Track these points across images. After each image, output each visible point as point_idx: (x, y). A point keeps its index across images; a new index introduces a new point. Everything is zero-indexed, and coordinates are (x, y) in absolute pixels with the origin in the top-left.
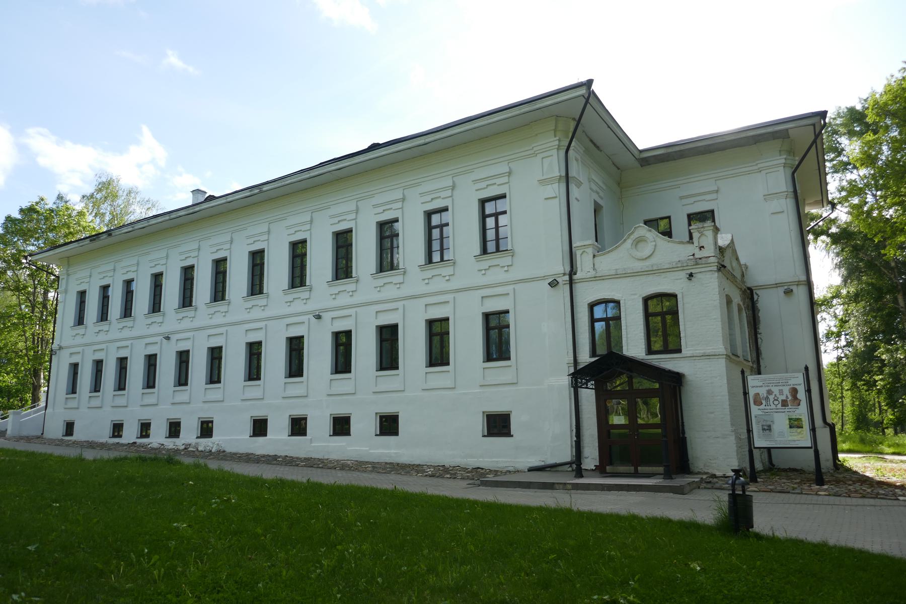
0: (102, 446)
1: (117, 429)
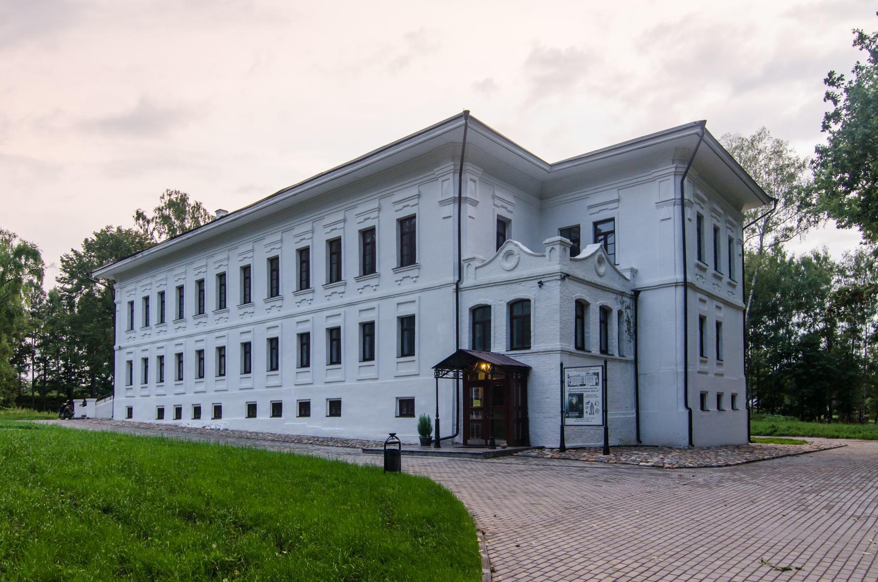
0: (149, 427)
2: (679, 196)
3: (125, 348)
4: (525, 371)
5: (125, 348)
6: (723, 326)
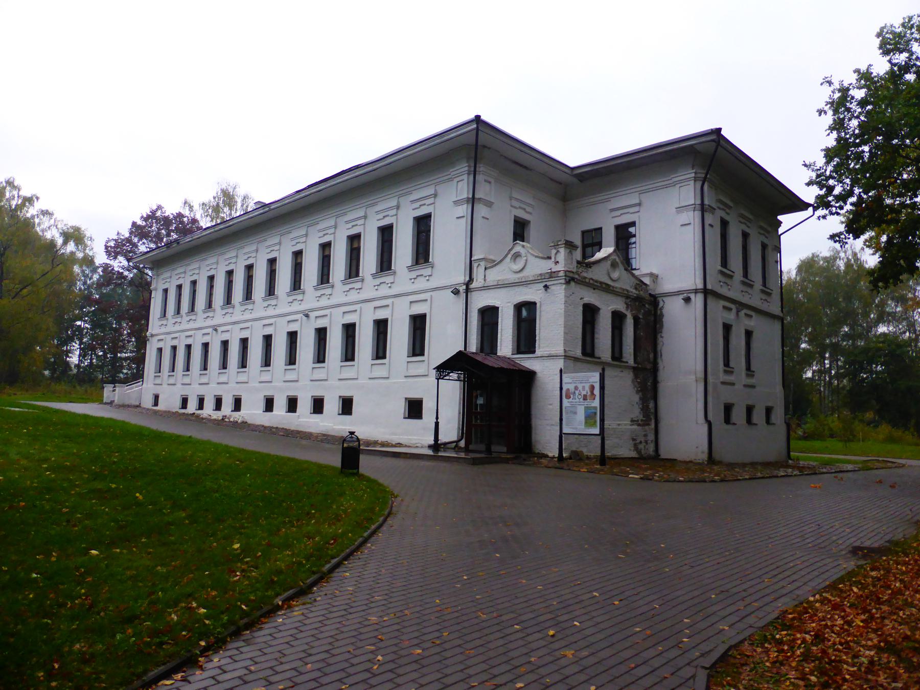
1: (185, 402)
2: (699, 202)
3: (156, 335)
4: (529, 376)
5: (156, 335)
6: (755, 335)
